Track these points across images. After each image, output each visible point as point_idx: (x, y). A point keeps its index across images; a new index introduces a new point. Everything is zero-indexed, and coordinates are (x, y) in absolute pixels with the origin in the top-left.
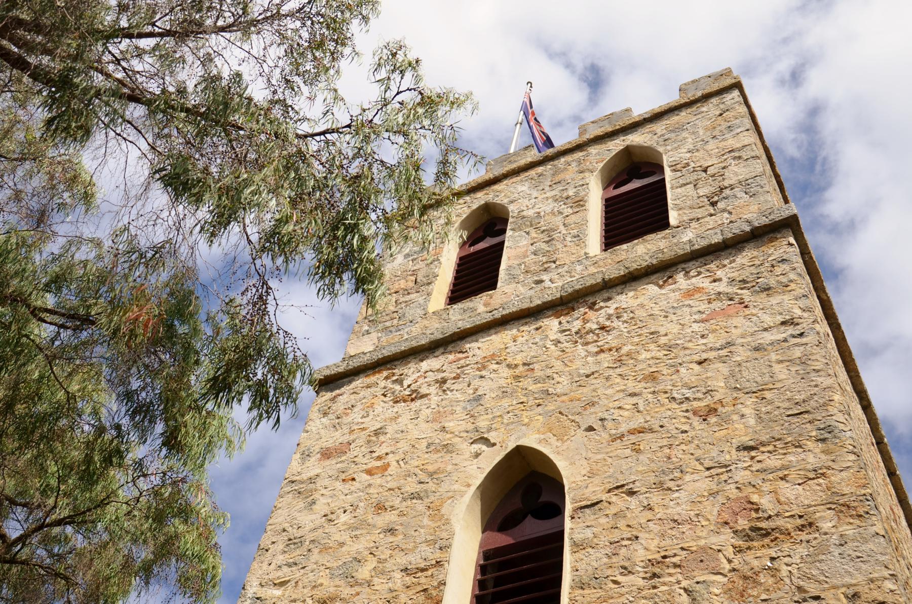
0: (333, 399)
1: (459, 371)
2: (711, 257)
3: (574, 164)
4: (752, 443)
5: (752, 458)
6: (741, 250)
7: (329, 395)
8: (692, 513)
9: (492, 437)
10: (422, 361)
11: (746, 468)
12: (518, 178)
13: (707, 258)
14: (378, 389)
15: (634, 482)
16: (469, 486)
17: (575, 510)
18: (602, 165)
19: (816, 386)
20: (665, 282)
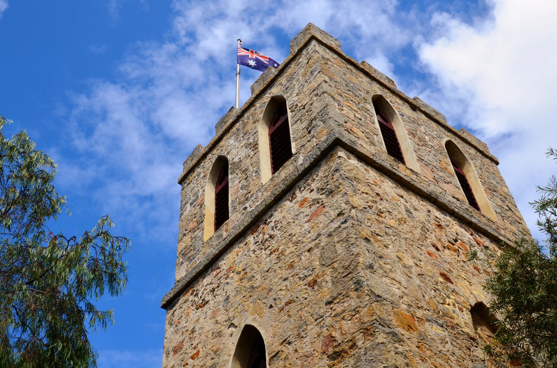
0: (173, 314)
1: (218, 282)
2: (309, 175)
3: (251, 117)
4: (330, 299)
5: (331, 309)
6: (319, 166)
7: (171, 312)
8: (312, 349)
9: (235, 322)
10: (204, 278)
11: (329, 316)
12: (229, 134)
13: (307, 176)
14: (189, 303)
15: (289, 337)
16: (230, 356)
17: (270, 360)
18: (262, 115)
19: (353, 254)
20: (292, 197)
